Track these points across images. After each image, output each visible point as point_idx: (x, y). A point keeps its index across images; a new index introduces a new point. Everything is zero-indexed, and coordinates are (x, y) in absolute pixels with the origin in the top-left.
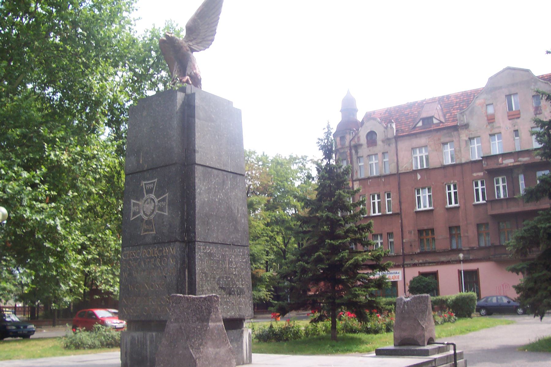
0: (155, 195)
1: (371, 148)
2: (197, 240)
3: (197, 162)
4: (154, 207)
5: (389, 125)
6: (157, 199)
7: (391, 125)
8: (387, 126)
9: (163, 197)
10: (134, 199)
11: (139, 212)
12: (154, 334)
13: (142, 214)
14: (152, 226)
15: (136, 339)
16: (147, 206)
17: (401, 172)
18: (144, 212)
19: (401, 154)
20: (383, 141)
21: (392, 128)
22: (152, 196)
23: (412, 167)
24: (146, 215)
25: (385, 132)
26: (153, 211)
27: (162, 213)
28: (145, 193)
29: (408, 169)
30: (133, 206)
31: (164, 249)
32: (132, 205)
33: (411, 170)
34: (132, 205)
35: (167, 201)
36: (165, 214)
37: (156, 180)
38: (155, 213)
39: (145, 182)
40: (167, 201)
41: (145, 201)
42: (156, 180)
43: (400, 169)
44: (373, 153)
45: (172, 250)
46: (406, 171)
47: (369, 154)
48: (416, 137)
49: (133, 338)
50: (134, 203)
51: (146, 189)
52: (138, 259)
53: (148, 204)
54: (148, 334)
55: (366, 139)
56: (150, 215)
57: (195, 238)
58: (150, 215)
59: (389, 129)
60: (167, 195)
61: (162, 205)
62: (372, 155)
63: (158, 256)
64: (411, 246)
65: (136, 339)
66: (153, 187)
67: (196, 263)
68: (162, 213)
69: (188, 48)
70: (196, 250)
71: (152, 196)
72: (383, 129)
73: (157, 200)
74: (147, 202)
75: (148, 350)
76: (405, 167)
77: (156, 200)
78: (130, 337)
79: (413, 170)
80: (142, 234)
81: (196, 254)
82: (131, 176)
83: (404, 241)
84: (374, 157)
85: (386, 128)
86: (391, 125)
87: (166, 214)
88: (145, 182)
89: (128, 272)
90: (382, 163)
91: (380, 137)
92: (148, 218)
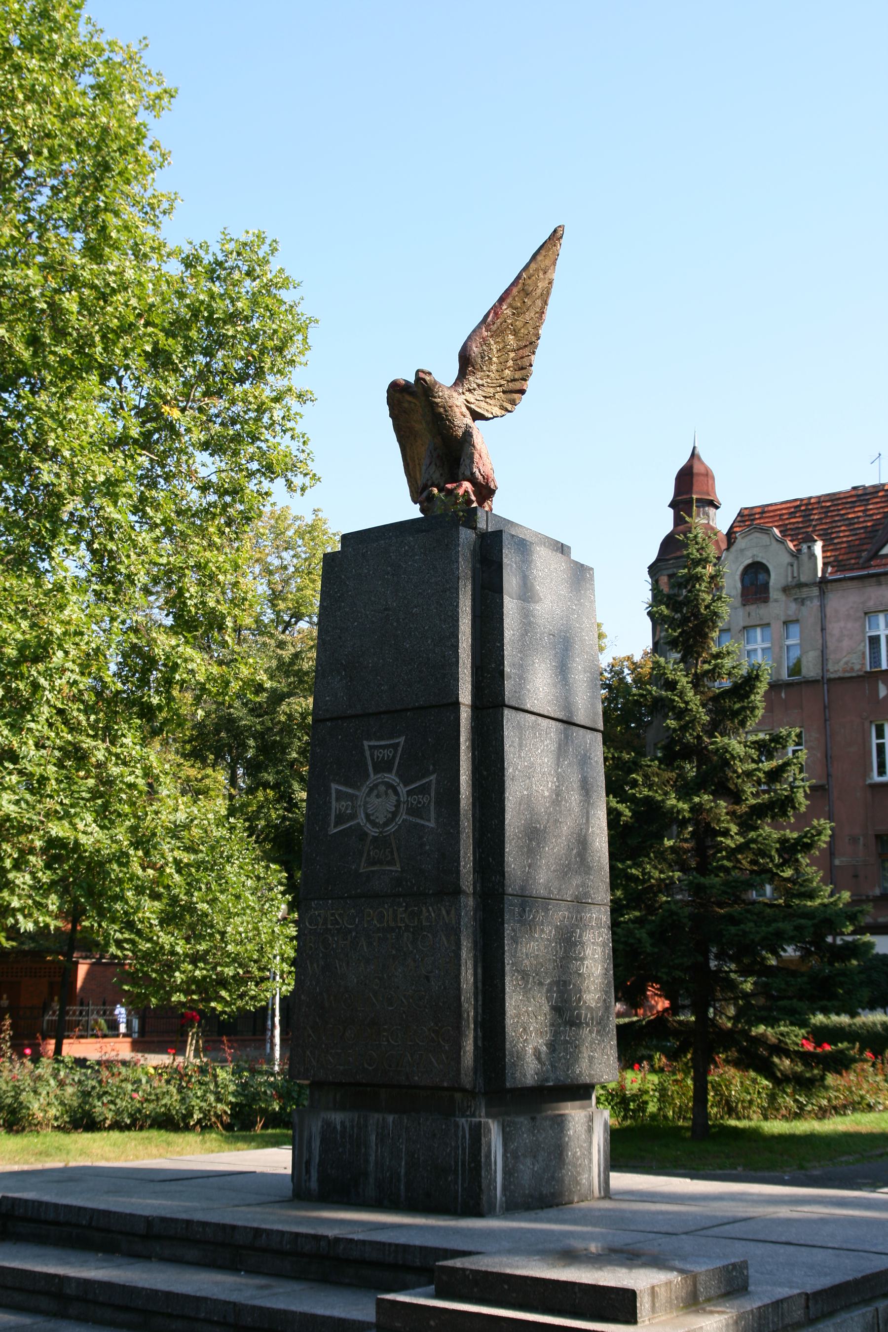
0: (398, 775)
1: (752, 608)
2: (507, 892)
3: (506, 702)
4: (397, 806)
5: (804, 547)
6: (405, 786)
7: (809, 547)
8: (799, 551)
9: (424, 781)
10: (338, 783)
11: (353, 816)
12: (390, 1118)
13: (361, 819)
14: (392, 853)
15: (339, 1127)
16: (377, 801)
17: (832, 676)
18: (367, 816)
19: (835, 628)
20: (786, 590)
21: (813, 556)
22: (392, 777)
23: (863, 664)
24: (374, 824)
25: (792, 566)
26: (395, 814)
27: (419, 821)
28: (370, 769)
29: (852, 669)
30: (337, 800)
31: (424, 909)
32: (334, 795)
33: (861, 673)
34: (334, 795)
35: (433, 794)
36: (427, 824)
37: (402, 740)
38: (399, 820)
39: (372, 743)
40: (433, 794)
41: (371, 790)
42: (402, 740)
43: (831, 667)
44: (758, 623)
45: (448, 913)
46: (847, 675)
47: (747, 624)
48: (879, 584)
49: (328, 1126)
50: (338, 792)
51: (372, 759)
52: (350, 931)
53: (378, 796)
54: (375, 1118)
55: (739, 585)
56: (386, 824)
57: (503, 885)
58: (386, 824)
59: (804, 558)
60: (433, 777)
61: (419, 802)
62: (754, 626)
63: (407, 926)
64: (856, 876)
65: (339, 1127)
66: (394, 757)
67: (506, 948)
68: (419, 821)
69: (464, 410)
70: (507, 917)
71: (392, 777)
72: (786, 559)
73: (405, 790)
74: (375, 793)
75: (372, 1158)
76: (846, 663)
77: (402, 790)
78: (320, 1124)
79: (866, 672)
80: (361, 871)
81: (506, 925)
82: (329, 724)
83: (837, 862)
84: (759, 630)
85: (796, 555)
86: (809, 547)
87: (432, 824)
88: (372, 743)
89: (322, 963)
90: (781, 648)
91: (776, 580)
92: (381, 833)
